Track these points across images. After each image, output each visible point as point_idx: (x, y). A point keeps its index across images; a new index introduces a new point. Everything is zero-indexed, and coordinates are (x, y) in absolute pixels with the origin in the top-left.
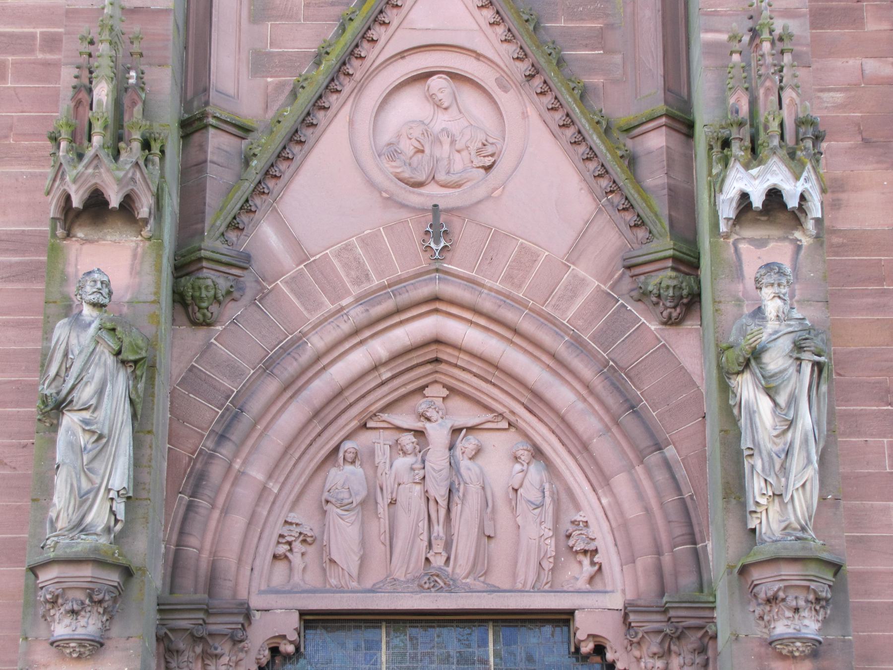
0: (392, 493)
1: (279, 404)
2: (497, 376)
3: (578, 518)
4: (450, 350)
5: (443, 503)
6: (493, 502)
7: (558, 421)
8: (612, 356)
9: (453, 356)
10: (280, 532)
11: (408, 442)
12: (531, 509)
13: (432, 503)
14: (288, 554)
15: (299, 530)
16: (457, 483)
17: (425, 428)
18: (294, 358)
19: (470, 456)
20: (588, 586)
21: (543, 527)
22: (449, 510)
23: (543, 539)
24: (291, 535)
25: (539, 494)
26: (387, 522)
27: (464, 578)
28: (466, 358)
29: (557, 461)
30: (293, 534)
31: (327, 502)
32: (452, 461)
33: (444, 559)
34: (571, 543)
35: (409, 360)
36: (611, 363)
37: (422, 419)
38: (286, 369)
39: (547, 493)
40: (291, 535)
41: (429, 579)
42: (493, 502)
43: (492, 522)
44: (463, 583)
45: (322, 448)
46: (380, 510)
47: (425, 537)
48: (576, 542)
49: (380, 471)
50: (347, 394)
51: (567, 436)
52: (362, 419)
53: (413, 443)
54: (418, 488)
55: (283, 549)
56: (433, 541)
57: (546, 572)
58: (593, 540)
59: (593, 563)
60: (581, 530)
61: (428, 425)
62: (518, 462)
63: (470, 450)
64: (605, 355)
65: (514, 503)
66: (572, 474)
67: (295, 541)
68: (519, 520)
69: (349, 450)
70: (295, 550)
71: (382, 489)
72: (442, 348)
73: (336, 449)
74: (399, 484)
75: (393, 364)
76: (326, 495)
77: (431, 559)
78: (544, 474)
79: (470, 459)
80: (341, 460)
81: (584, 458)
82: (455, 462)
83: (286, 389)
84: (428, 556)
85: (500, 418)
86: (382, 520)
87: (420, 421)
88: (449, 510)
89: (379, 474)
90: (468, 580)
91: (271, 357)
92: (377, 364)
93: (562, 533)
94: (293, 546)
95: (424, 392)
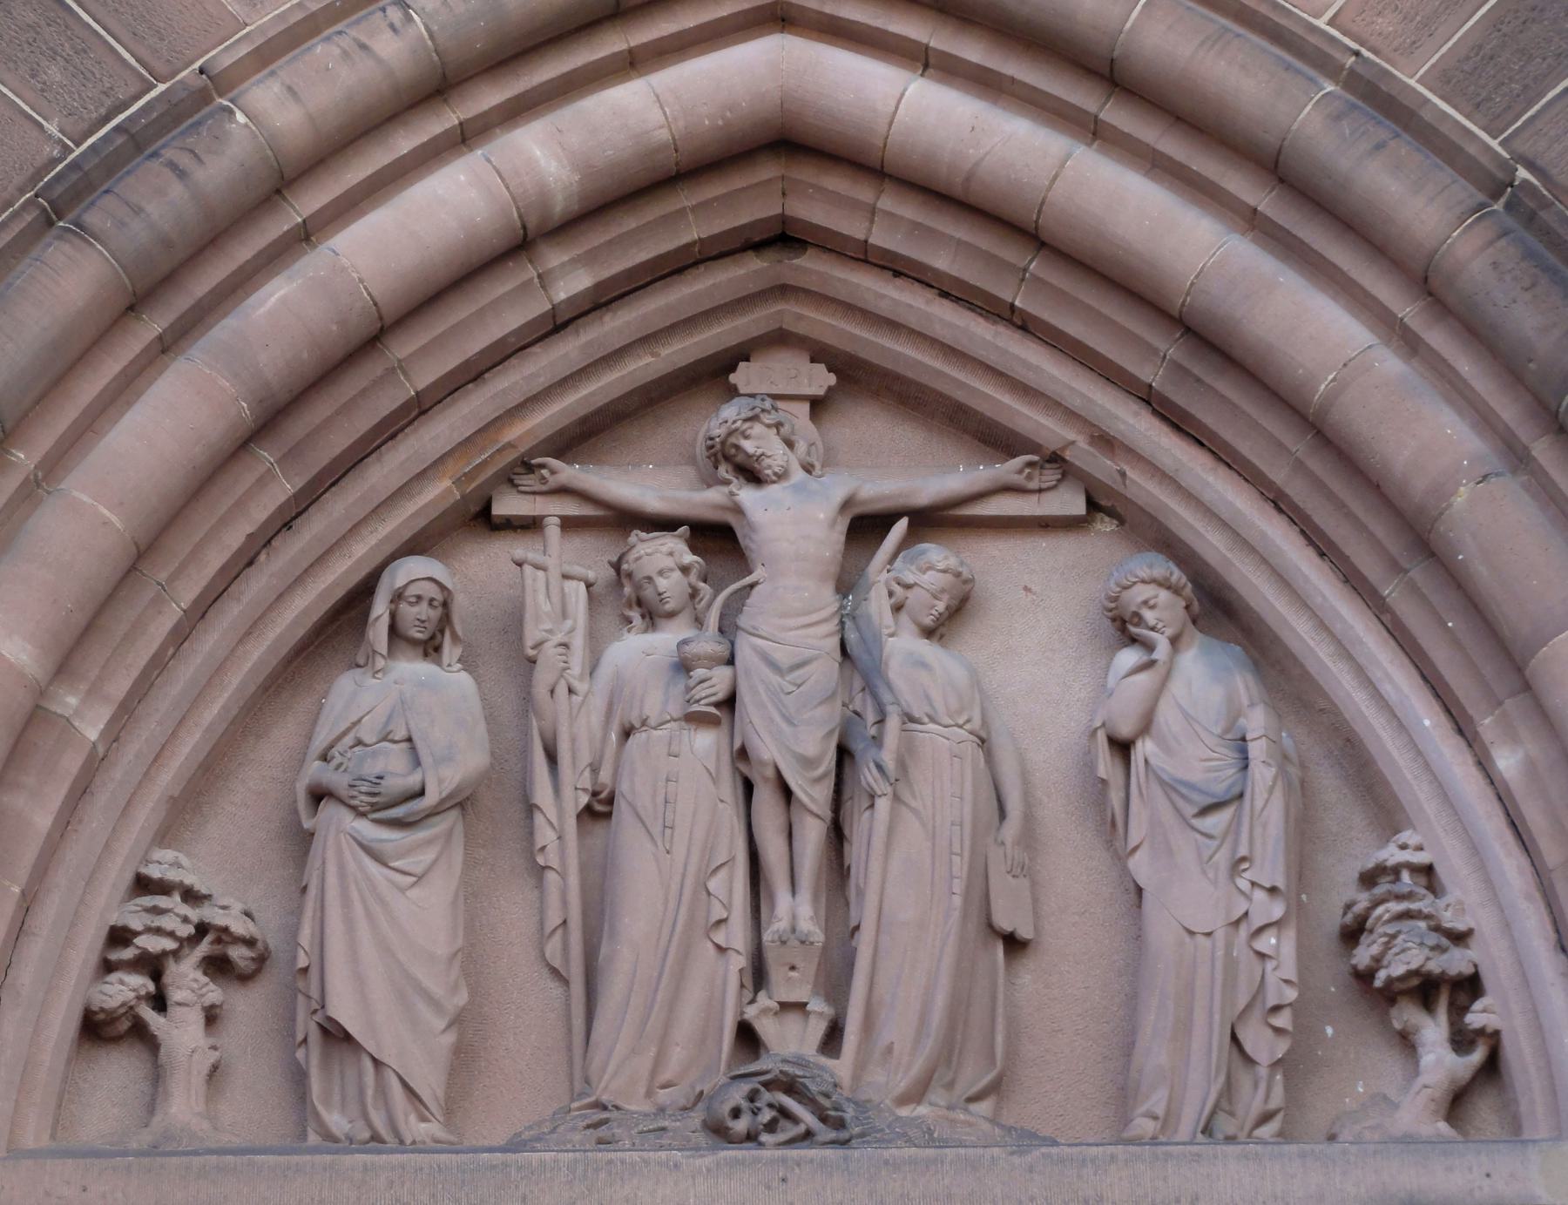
0: (595, 769)
1: (110, 367)
2: (1036, 278)
3: (1392, 855)
4: (837, 182)
5: (814, 794)
6: (1027, 795)
7: (1299, 445)
8: (1523, 146)
9: (854, 205)
10: (115, 919)
11: (669, 562)
12: (1190, 810)
13: (765, 797)
14: (148, 1014)
15: (195, 914)
16: (871, 717)
17: (738, 510)
18: (172, 166)
19: (928, 621)
20: (1443, 1126)
21: (1243, 884)
22: (837, 834)
23: (1243, 932)
24: (159, 931)
25: (1227, 758)
26: (574, 880)
27: (904, 1100)
28: (908, 209)
29: (1296, 629)
30: (168, 923)
31: (318, 796)
32: (852, 637)
33: (817, 1029)
34: (1363, 955)
35: (667, 220)
36: (1522, 173)
37: (724, 471)
38: (138, 211)
39: (1257, 750)
40: (159, 931)
41: (752, 1097)
42: (1027, 795)
43: (1025, 882)
44: (898, 1118)
45: (299, 581)
46: (545, 835)
47: (737, 935)
48: (1387, 946)
49: (543, 677)
50: (402, 347)
51: (1341, 506)
52: (469, 476)
53: (685, 570)
54: (705, 741)
55: (126, 988)
56: (771, 956)
57: (1263, 1071)
58: (1460, 938)
59: (1461, 1040)
60: (1409, 896)
61: (747, 496)
62: (1134, 640)
63: (929, 600)
64: (1494, 144)
65: (1116, 797)
66: (1360, 672)
67: (175, 954)
68: (1140, 866)
69: (413, 591)
70: (175, 995)
71: (552, 757)
72: (806, 173)
73: (360, 596)
74: (627, 733)
75: (596, 237)
76: (314, 771)
77: (767, 1028)
78: (1244, 684)
79: (929, 633)
80: (378, 633)
81: (1414, 589)
82: (863, 639)
83: (135, 304)
84: (751, 1013)
85: (1050, 476)
86: (551, 877)
87: (712, 481)
88: (837, 834)
89: (540, 690)
90: (922, 1110)
91: (75, 165)
92: (532, 223)
93: (1334, 920)
94: (167, 979)
95: (733, 378)
